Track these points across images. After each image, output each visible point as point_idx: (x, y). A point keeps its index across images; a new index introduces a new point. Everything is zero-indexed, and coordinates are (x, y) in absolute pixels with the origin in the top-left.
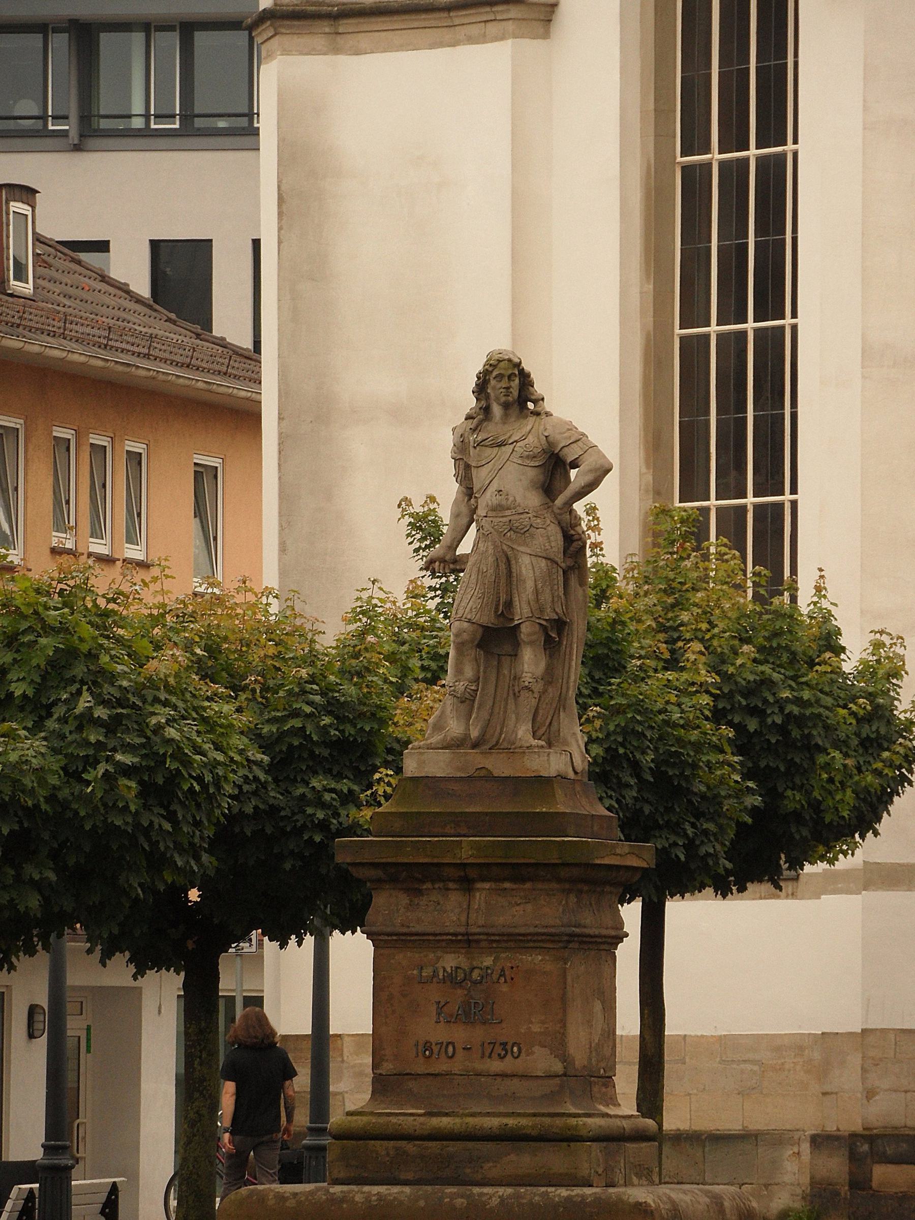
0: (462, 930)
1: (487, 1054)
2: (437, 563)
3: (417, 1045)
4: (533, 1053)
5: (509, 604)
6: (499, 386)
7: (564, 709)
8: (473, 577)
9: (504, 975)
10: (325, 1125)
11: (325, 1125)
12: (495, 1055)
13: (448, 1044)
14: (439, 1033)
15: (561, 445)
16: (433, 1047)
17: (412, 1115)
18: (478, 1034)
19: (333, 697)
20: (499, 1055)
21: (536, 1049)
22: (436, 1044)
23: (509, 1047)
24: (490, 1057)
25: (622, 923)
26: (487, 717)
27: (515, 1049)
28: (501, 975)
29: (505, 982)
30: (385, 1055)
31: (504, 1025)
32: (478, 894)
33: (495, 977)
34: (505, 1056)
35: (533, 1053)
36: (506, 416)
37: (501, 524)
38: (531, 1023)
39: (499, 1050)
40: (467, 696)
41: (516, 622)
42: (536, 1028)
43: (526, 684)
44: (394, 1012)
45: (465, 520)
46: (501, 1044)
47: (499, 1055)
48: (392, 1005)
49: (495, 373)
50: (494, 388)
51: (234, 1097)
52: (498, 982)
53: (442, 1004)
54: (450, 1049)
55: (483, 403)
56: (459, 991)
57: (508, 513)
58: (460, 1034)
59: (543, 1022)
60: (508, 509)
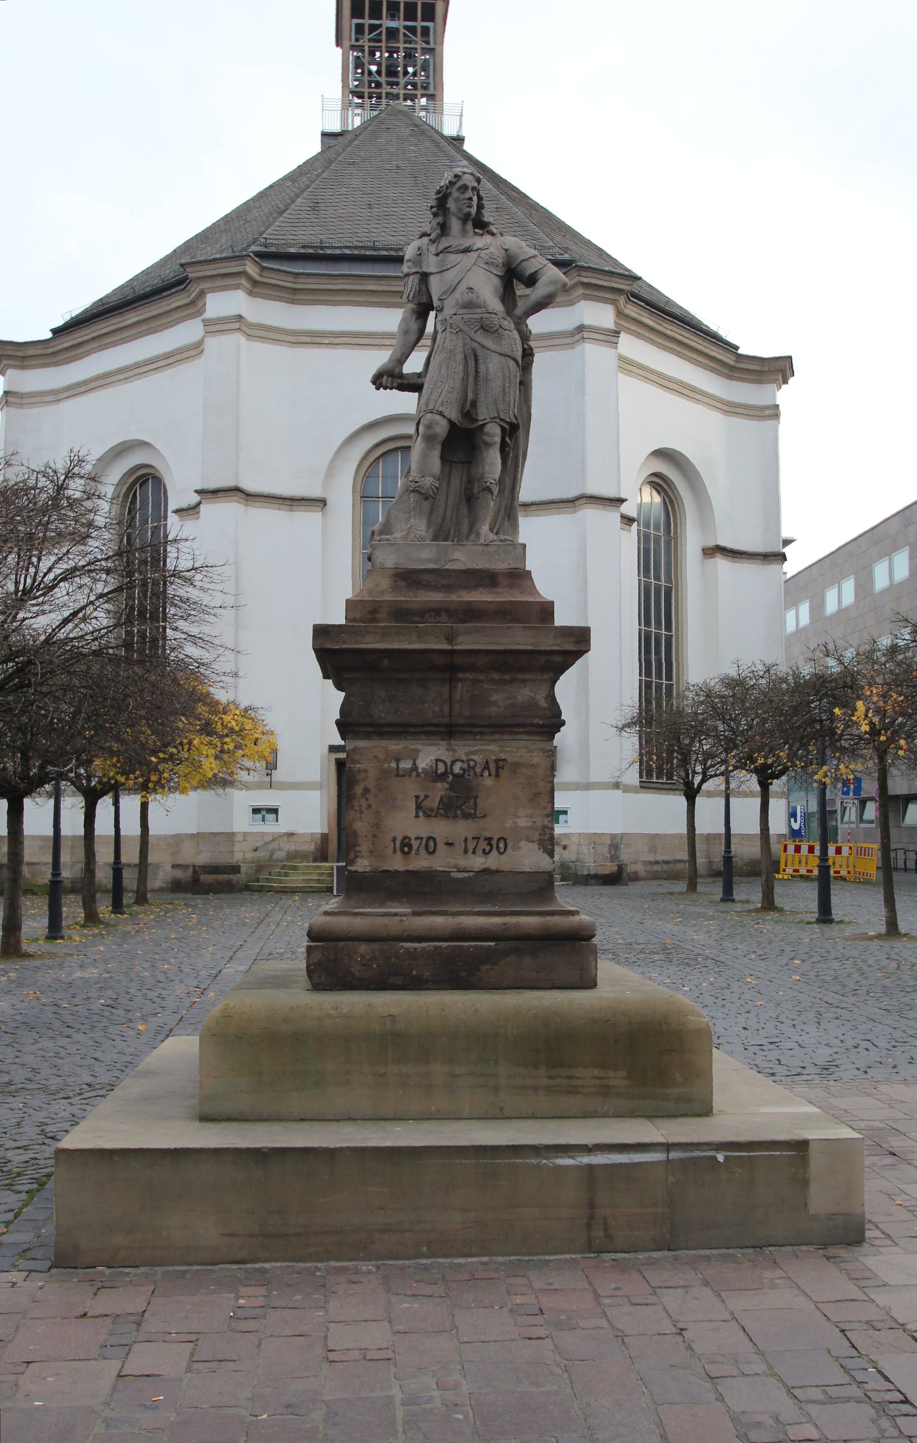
0: (445, 720)
1: (471, 849)
2: (385, 378)
3: (394, 840)
4: (519, 848)
5: (474, 404)
6: (462, 197)
7: (509, 519)
8: (443, 372)
9: (488, 768)
10: (311, 944)
11: (311, 944)
12: (479, 851)
13: (429, 838)
14: (415, 827)
15: (521, 258)
16: (413, 842)
17: (396, 914)
18: (461, 829)
19: (71, 759)
20: (484, 850)
21: (523, 844)
22: (416, 838)
23: (494, 842)
24: (474, 853)
25: (559, 713)
26: (440, 521)
27: (502, 845)
28: (485, 768)
29: (490, 775)
30: (360, 852)
31: (488, 819)
32: (460, 685)
33: (478, 770)
34: (490, 851)
35: (519, 848)
36: (464, 232)
37: (473, 321)
38: (518, 817)
39: (483, 845)
40: (431, 493)
41: (480, 423)
42: (522, 822)
43: (488, 484)
44: (370, 806)
45: (413, 338)
46: (486, 839)
47: (484, 850)
48: (367, 799)
49: (458, 185)
50: (457, 200)
51: (211, 896)
52: (482, 775)
53: (422, 797)
54: (431, 844)
55: (440, 219)
56: (439, 785)
57: (479, 311)
58: (441, 828)
59: (531, 816)
60: (480, 307)
